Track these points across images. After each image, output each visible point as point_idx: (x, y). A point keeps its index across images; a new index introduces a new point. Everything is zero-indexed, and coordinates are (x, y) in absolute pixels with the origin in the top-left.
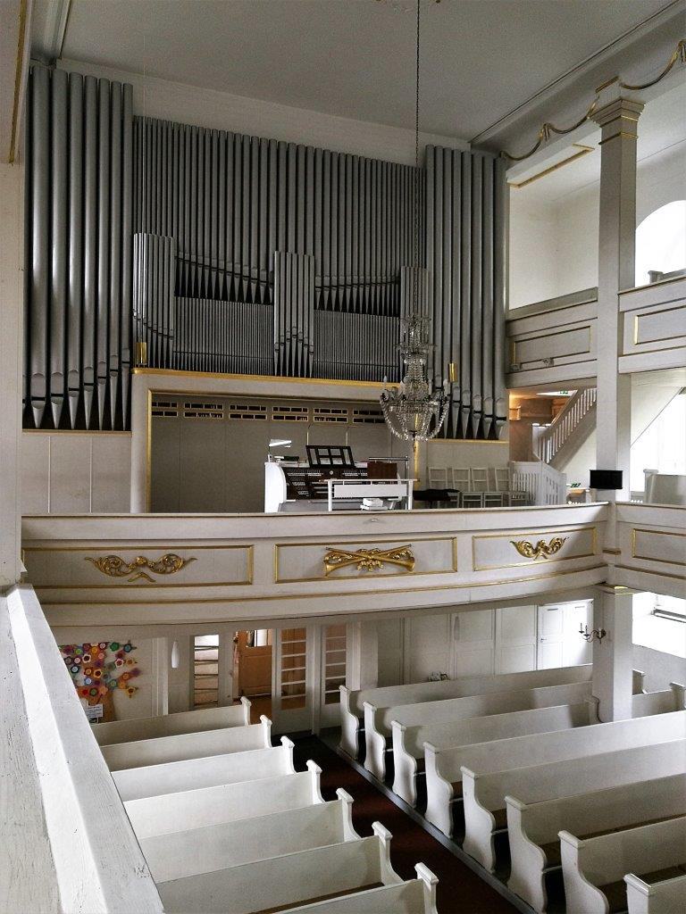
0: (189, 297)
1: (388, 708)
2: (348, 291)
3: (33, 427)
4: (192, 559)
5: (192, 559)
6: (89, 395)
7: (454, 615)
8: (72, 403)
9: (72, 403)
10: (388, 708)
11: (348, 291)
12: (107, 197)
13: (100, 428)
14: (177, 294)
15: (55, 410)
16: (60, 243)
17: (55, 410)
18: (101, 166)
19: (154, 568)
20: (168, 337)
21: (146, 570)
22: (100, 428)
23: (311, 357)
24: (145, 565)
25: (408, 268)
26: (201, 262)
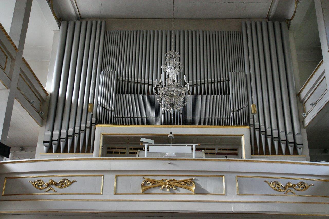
0: (133, 94)
1: (198, 180)
2: (202, 86)
3: (282, 154)
4: (74, 182)
5: (74, 182)
6: (77, 138)
7: (50, 200)
8: (69, 141)
9: (69, 141)
10: (198, 180)
11: (202, 86)
12: (126, 63)
13: (277, 153)
14: (116, 93)
15: (62, 145)
16: (78, 77)
17: (62, 145)
18: (137, 52)
19: (56, 184)
20: (112, 111)
21: (54, 187)
22: (277, 153)
23: (181, 115)
24: (52, 184)
25: (233, 72)
26: (143, 82)
